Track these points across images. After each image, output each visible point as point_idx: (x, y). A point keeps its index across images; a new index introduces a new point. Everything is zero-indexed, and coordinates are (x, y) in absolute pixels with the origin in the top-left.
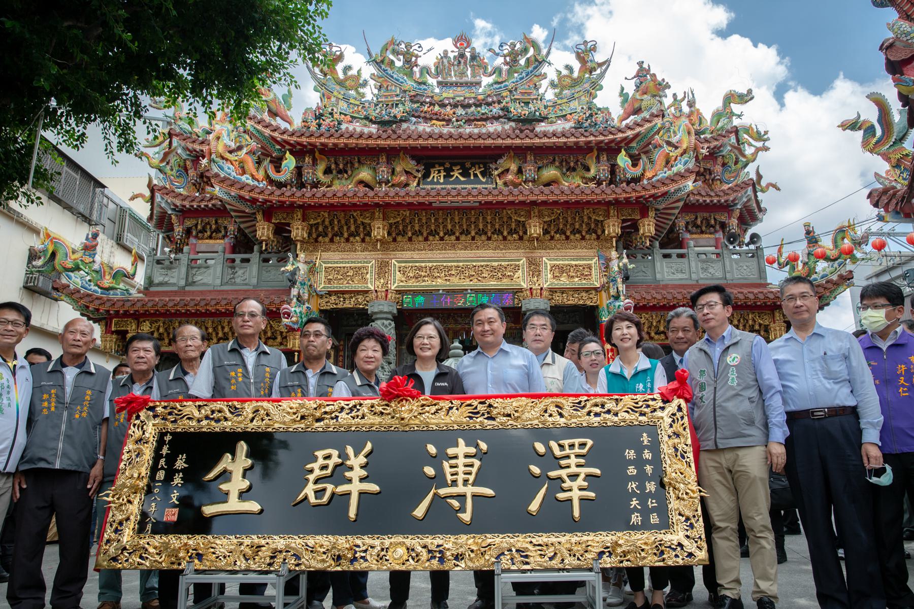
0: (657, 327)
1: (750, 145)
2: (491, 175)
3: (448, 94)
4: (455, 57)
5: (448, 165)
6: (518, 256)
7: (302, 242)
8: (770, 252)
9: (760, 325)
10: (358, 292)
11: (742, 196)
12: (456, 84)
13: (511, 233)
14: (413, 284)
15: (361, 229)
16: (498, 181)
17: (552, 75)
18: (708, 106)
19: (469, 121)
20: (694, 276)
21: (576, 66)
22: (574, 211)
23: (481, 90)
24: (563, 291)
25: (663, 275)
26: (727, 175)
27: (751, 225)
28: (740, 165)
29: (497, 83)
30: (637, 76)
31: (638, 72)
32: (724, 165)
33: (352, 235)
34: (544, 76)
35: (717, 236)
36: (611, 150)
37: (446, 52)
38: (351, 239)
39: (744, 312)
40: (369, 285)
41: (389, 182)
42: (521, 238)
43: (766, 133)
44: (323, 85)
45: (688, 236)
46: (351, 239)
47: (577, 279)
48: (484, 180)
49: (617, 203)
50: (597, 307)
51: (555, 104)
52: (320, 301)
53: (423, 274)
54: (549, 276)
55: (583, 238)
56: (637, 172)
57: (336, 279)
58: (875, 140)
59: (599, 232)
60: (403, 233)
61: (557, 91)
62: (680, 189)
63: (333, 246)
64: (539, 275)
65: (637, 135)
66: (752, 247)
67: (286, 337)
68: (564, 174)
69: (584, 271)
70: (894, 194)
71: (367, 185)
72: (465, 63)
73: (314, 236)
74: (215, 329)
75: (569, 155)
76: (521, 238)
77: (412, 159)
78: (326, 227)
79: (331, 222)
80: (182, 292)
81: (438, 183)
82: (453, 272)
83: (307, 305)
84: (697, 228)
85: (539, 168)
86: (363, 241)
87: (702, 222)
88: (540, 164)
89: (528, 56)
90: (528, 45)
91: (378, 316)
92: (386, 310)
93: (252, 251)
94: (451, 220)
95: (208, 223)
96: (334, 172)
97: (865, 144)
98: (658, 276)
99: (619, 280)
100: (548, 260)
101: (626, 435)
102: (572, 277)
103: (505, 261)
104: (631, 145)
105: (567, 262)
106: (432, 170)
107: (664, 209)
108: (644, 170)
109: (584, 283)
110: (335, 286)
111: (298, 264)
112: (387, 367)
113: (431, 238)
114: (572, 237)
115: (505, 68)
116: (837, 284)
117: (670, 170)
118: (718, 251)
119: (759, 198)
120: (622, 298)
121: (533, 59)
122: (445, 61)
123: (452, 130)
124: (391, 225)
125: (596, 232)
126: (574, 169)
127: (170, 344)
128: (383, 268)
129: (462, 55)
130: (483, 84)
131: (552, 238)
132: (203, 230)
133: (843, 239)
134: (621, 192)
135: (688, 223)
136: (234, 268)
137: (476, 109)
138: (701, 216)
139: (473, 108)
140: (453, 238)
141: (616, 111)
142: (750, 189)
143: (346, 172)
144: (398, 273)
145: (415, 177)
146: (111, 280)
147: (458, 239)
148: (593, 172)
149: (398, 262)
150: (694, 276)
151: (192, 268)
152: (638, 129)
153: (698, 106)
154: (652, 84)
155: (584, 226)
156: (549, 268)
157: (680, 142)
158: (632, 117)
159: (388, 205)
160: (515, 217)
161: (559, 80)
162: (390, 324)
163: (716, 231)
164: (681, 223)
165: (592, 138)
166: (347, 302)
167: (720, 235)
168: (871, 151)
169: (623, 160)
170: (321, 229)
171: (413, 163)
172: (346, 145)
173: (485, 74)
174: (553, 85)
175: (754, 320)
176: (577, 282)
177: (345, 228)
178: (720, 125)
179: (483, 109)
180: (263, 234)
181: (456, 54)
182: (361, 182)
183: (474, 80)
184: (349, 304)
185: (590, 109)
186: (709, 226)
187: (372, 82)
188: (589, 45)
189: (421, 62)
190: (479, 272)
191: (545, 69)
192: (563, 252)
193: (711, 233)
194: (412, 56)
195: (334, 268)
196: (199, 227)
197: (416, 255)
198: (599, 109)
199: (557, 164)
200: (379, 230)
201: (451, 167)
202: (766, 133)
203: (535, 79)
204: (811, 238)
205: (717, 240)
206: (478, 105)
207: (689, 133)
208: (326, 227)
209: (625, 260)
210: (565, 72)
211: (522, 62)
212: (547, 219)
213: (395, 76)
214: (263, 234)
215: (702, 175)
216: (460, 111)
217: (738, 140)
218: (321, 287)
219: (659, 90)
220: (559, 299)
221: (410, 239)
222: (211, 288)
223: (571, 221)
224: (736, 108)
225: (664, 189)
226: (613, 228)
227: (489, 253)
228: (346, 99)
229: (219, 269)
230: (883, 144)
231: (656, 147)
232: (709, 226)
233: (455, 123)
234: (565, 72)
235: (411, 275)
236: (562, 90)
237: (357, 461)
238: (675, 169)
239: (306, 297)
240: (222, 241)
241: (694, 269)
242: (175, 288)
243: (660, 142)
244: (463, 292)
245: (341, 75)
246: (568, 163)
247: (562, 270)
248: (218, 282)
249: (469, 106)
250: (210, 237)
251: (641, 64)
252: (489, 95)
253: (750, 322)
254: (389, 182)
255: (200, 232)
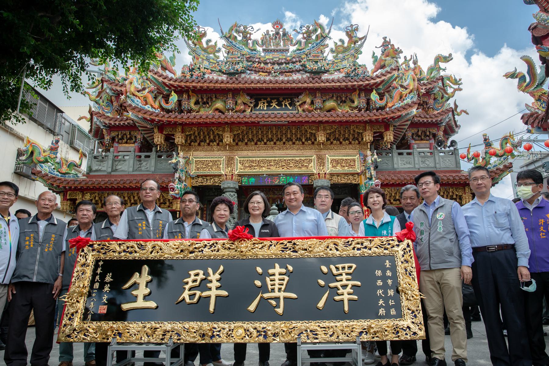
0: (394, 196)
1: (451, 87)
2: (295, 105)
3: (269, 56)
4: (273, 34)
5: (269, 99)
6: (311, 154)
7: (181, 145)
8: (462, 152)
9: (457, 195)
10: (215, 176)
11: (446, 118)
12: (274, 51)
13: (307, 140)
14: (248, 171)
15: (217, 138)
16: (299, 109)
17: (331, 45)
18: (425, 64)
19: (282, 73)
20: (417, 166)
21: (346, 39)
22: (345, 127)
23: (289, 54)
24: (338, 175)
25: (398, 165)
26: (437, 105)
27: (451, 135)
28: (444, 99)
29: (298, 50)
30: (383, 45)
31: (383, 43)
32: (435, 99)
33: (211, 141)
34: (327, 46)
35: (431, 142)
36: (367, 90)
37: (268, 31)
38: (211, 143)
39: (447, 188)
40: (222, 171)
41: (233, 109)
42: (313, 143)
43: (460, 80)
44: (194, 51)
45: (413, 142)
46: (211, 143)
47: (346, 168)
48: (291, 108)
49: (370, 122)
50: (359, 184)
51: (333, 63)
52: (192, 181)
53: (254, 165)
54: (330, 166)
55: (350, 143)
56: (383, 103)
57: (202, 168)
58: (525, 84)
59: (360, 140)
60: (242, 140)
61: (335, 54)
62: (408, 114)
63: (200, 148)
64: (324, 165)
65: (383, 81)
66: (452, 148)
67: (172, 203)
68: (339, 105)
69: (351, 163)
70: (537, 117)
71: (220, 111)
72: (279, 38)
73: (189, 142)
74: (129, 198)
75: (342, 93)
76: (313, 143)
77: (248, 96)
78: (196, 137)
79: (199, 134)
80: (109, 175)
81: (263, 110)
82: (272, 164)
83: (184, 183)
84: (419, 137)
85: (324, 101)
86: (218, 145)
87: (421, 134)
88: (324, 98)
89: (317, 33)
90: (317, 27)
91: (227, 190)
92: (232, 186)
93: (151, 151)
94: (271, 132)
95: (125, 134)
96: (201, 103)
97: (520, 86)
98: (395, 166)
99: (372, 168)
100: (329, 156)
101: (376, 262)
102: (344, 166)
103: (303, 157)
104: (379, 87)
105: (340, 158)
106: (260, 102)
107: (399, 125)
108: (387, 102)
109: (351, 170)
110: (201, 172)
111: (179, 159)
112: (232, 221)
113: (259, 143)
114: (344, 142)
115: (303, 41)
116: (503, 171)
117: (402, 102)
118: (431, 151)
119: (456, 119)
120: (374, 179)
121: (320, 35)
122: (267, 36)
123: (272, 78)
124: (235, 135)
125: (358, 140)
126: (345, 102)
127: (102, 207)
128: (230, 161)
129: (277, 33)
130: (290, 50)
131: (332, 143)
132: (122, 138)
133: (506, 143)
134: (373, 115)
135: (413, 134)
136: (140, 161)
137: (286, 66)
138: (421, 130)
139: (284, 65)
140: (272, 143)
141: (370, 67)
142: (451, 113)
143: (208, 104)
144: (239, 164)
145: (249, 106)
146: (67, 168)
147: (275, 143)
148: (356, 103)
149: (239, 157)
150: (417, 166)
151: (115, 161)
152: (383, 78)
153: (419, 63)
154: (391, 50)
155: (351, 136)
156: (330, 161)
157: (408, 85)
158: (380, 70)
159: (233, 123)
160: (309, 131)
161: (336, 48)
162: (234, 195)
163: (430, 139)
164: (409, 134)
165: (355, 83)
166: (209, 182)
167: (432, 141)
168: (523, 91)
169: (374, 96)
170: (193, 138)
171: (248, 98)
172: (208, 87)
173: (291, 44)
174: (332, 51)
175: (453, 193)
176: (347, 170)
177: (207, 137)
178: (432, 75)
179: (290, 66)
180: (158, 141)
181: (274, 32)
182: (217, 109)
183: (285, 48)
184: (210, 183)
185: (354, 65)
186: (426, 136)
187: (223, 50)
188: (354, 27)
189: (253, 37)
190: (287, 163)
191: (327, 41)
192: (338, 152)
193: (427, 140)
194: (248, 33)
195: (200, 161)
196: (120, 137)
197: (250, 153)
198: (360, 66)
199: (335, 98)
200: (228, 138)
201: (271, 101)
202: (460, 80)
203: (322, 47)
204: (487, 143)
205: (431, 144)
206: (287, 63)
207: (414, 80)
208: (196, 137)
209: (376, 156)
210: (339, 43)
211: (314, 37)
212: (328, 132)
213: (237, 46)
214: (158, 141)
215: (422, 105)
216: (276, 67)
217: (443, 84)
218: (193, 172)
219: (396, 54)
220: (336, 180)
221: (246, 144)
222: (127, 173)
223: (343, 133)
224: (442, 65)
225: (399, 114)
226: (368, 137)
227: (294, 152)
228: (208, 59)
229: (132, 162)
230: (531, 87)
231: (394, 88)
232: (426, 136)
233: (273, 74)
234: (339, 43)
235: (247, 165)
236: (337, 54)
237: (214, 277)
238: (405, 102)
239: (184, 178)
240: (133, 145)
241: (417, 162)
242: (105, 173)
243: (397, 85)
244: (278, 175)
245: (205, 45)
246: (341, 98)
247: (337, 162)
248: (131, 169)
249: (282, 64)
250: (126, 143)
251: (385, 38)
252: (294, 57)
253: (451, 194)
254: (233, 109)
255: (120, 139)
